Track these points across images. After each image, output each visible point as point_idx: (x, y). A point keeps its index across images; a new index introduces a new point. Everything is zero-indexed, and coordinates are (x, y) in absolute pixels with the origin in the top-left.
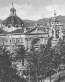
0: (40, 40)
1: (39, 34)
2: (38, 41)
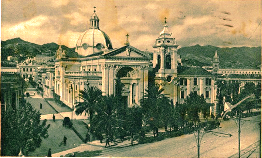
0: (133, 70)
1: (132, 59)
2: (129, 72)
